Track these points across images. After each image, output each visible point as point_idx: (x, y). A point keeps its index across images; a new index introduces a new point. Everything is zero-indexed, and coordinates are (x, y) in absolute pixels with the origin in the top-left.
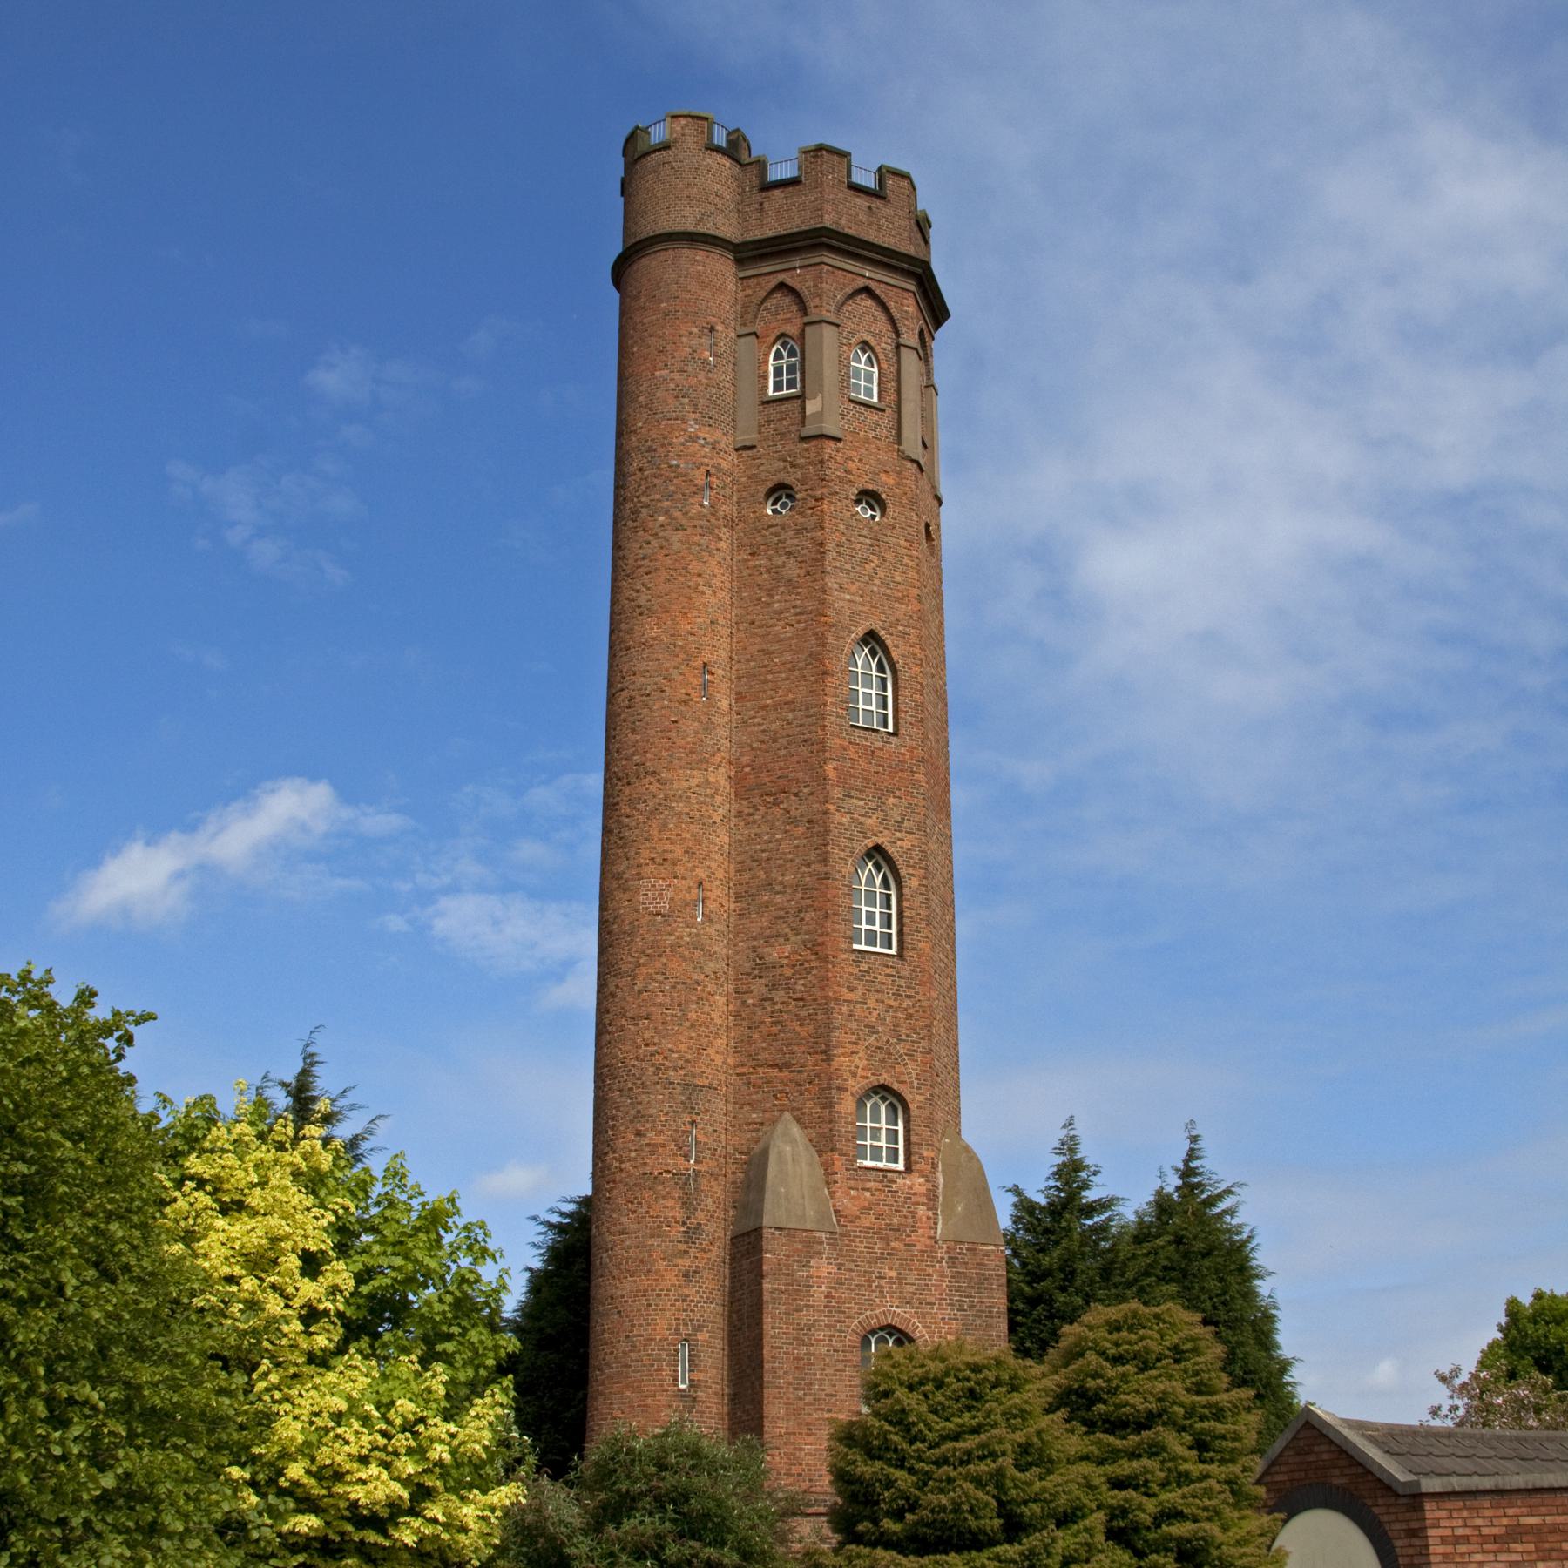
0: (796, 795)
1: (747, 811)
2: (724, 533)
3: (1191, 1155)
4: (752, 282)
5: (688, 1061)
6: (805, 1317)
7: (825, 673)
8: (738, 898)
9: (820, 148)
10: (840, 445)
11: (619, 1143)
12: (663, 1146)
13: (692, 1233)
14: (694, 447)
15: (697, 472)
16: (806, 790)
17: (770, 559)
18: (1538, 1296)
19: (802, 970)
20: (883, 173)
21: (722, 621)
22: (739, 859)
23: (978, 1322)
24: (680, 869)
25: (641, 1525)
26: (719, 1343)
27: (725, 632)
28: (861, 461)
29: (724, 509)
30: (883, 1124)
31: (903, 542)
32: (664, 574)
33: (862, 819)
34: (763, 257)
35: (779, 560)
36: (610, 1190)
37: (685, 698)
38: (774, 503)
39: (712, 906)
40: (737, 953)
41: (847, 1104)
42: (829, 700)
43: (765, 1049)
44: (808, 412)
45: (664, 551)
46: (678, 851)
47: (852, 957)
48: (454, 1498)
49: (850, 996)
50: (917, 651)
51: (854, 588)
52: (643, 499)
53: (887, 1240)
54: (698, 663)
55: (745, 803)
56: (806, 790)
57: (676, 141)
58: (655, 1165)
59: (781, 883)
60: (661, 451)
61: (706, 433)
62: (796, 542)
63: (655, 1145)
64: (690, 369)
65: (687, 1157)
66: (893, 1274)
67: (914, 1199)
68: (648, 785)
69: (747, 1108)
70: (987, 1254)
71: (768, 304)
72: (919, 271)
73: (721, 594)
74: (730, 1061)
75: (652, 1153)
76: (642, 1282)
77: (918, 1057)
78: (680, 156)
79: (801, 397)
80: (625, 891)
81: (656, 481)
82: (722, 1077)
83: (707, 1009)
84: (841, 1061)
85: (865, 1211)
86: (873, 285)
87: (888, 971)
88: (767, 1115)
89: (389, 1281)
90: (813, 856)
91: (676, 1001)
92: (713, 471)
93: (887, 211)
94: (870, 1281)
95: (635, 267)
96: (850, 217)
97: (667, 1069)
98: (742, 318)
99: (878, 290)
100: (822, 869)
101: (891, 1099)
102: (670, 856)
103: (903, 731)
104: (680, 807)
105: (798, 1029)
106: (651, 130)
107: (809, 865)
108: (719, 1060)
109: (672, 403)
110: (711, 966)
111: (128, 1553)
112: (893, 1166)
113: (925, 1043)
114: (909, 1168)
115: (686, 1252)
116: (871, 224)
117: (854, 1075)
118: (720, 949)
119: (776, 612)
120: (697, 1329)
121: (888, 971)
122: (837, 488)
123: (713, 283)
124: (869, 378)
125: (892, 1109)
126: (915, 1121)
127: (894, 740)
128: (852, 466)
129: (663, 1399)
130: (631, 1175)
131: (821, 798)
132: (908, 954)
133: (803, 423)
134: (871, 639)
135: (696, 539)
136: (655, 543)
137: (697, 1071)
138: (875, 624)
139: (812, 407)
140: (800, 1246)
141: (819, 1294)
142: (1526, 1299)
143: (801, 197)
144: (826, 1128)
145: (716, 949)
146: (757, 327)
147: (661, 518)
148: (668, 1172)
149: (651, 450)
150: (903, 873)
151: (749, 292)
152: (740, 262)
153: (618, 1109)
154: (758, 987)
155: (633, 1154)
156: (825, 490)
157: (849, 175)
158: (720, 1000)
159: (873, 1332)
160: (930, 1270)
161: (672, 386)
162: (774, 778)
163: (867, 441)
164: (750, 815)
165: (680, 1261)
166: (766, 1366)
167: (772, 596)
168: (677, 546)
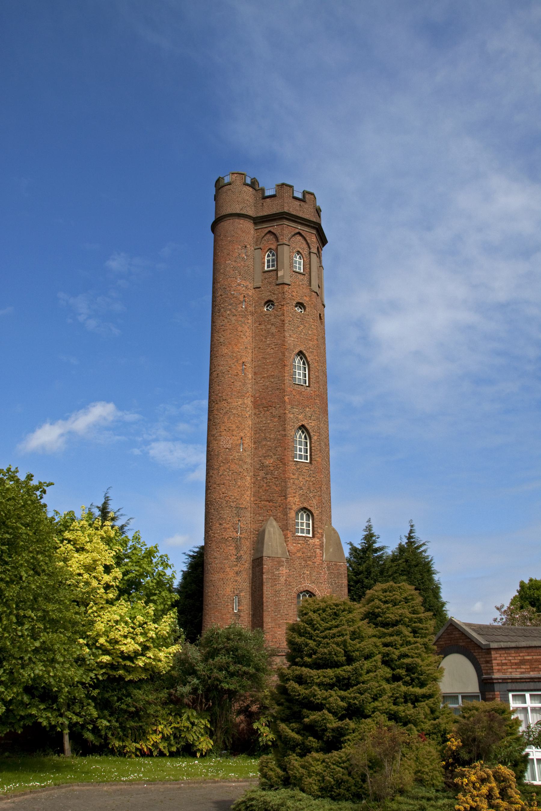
0: (275, 407)
1: (258, 413)
2: (250, 317)
3: (411, 532)
4: (260, 230)
5: (237, 499)
6: (278, 587)
7: (285, 365)
8: (255, 443)
9: (283, 184)
10: (290, 287)
11: (214, 528)
12: (229, 528)
13: (239, 558)
15: (240, 296)
17: (266, 326)
19: (277, 468)
20: (305, 193)
21: (249, 348)
22: (255, 429)
23: (338, 589)
24: (234, 433)
25: (221, 659)
27: (250, 351)
28: (297, 292)
29: (250, 309)
31: (311, 320)
32: (229, 331)
33: (297, 416)
35: (269, 327)
36: (211, 544)
37: (236, 374)
38: (267, 307)
39: (246, 446)
40: (254, 462)
41: (292, 514)
42: (286, 375)
43: (264, 495)
44: (279, 276)
45: (229, 323)
46: (234, 427)
47: (294, 463)
49: (293, 477)
51: (295, 336)
52: (222, 305)
53: (306, 561)
54: (241, 362)
55: (257, 410)
57: (233, 182)
58: (226, 535)
59: (269, 438)
60: (228, 289)
61: (243, 283)
62: (275, 320)
63: (226, 528)
65: (237, 532)
66: (308, 572)
67: (315, 547)
68: (224, 404)
69: (258, 515)
70: (341, 566)
71: (265, 238)
72: (317, 227)
73: (249, 338)
74: (252, 499)
75: (225, 531)
76: (221, 575)
77: (317, 498)
79: (276, 270)
80: (216, 441)
81: (226, 299)
82: (249, 505)
84: (290, 499)
85: (298, 551)
86: (301, 232)
87: (306, 468)
88: (265, 518)
89: (134, 575)
92: (246, 296)
93: (306, 206)
94: (300, 575)
96: (293, 208)
97: (230, 502)
98: (256, 243)
100: (283, 433)
101: (307, 512)
102: (231, 429)
103: (311, 385)
104: (234, 412)
105: (275, 488)
107: (279, 432)
108: (248, 499)
109: (232, 272)
110: (245, 466)
111: (44, 669)
112: (308, 535)
113: (319, 493)
114: (314, 536)
116: (300, 211)
117: (295, 504)
118: (249, 460)
120: (241, 592)
121: (306, 468)
122: (289, 302)
124: (300, 264)
125: (308, 516)
126: (316, 520)
127: (308, 388)
128: (294, 294)
129: (229, 616)
131: (283, 408)
132: (313, 462)
133: (277, 279)
134: (301, 354)
136: (226, 321)
137: (240, 502)
139: (280, 274)
140: (276, 563)
141: (283, 579)
143: (276, 201)
144: (285, 522)
146: (261, 246)
148: (230, 537)
149: (225, 288)
150: (312, 434)
151: (258, 234)
152: (255, 224)
153: (213, 516)
154: (262, 474)
155: (218, 531)
156: (285, 302)
157: (293, 194)
158: (248, 478)
159: (301, 593)
160: (321, 571)
164: (259, 414)
165: (235, 568)
166: (264, 604)
167: (266, 339)
168: (234, 321)
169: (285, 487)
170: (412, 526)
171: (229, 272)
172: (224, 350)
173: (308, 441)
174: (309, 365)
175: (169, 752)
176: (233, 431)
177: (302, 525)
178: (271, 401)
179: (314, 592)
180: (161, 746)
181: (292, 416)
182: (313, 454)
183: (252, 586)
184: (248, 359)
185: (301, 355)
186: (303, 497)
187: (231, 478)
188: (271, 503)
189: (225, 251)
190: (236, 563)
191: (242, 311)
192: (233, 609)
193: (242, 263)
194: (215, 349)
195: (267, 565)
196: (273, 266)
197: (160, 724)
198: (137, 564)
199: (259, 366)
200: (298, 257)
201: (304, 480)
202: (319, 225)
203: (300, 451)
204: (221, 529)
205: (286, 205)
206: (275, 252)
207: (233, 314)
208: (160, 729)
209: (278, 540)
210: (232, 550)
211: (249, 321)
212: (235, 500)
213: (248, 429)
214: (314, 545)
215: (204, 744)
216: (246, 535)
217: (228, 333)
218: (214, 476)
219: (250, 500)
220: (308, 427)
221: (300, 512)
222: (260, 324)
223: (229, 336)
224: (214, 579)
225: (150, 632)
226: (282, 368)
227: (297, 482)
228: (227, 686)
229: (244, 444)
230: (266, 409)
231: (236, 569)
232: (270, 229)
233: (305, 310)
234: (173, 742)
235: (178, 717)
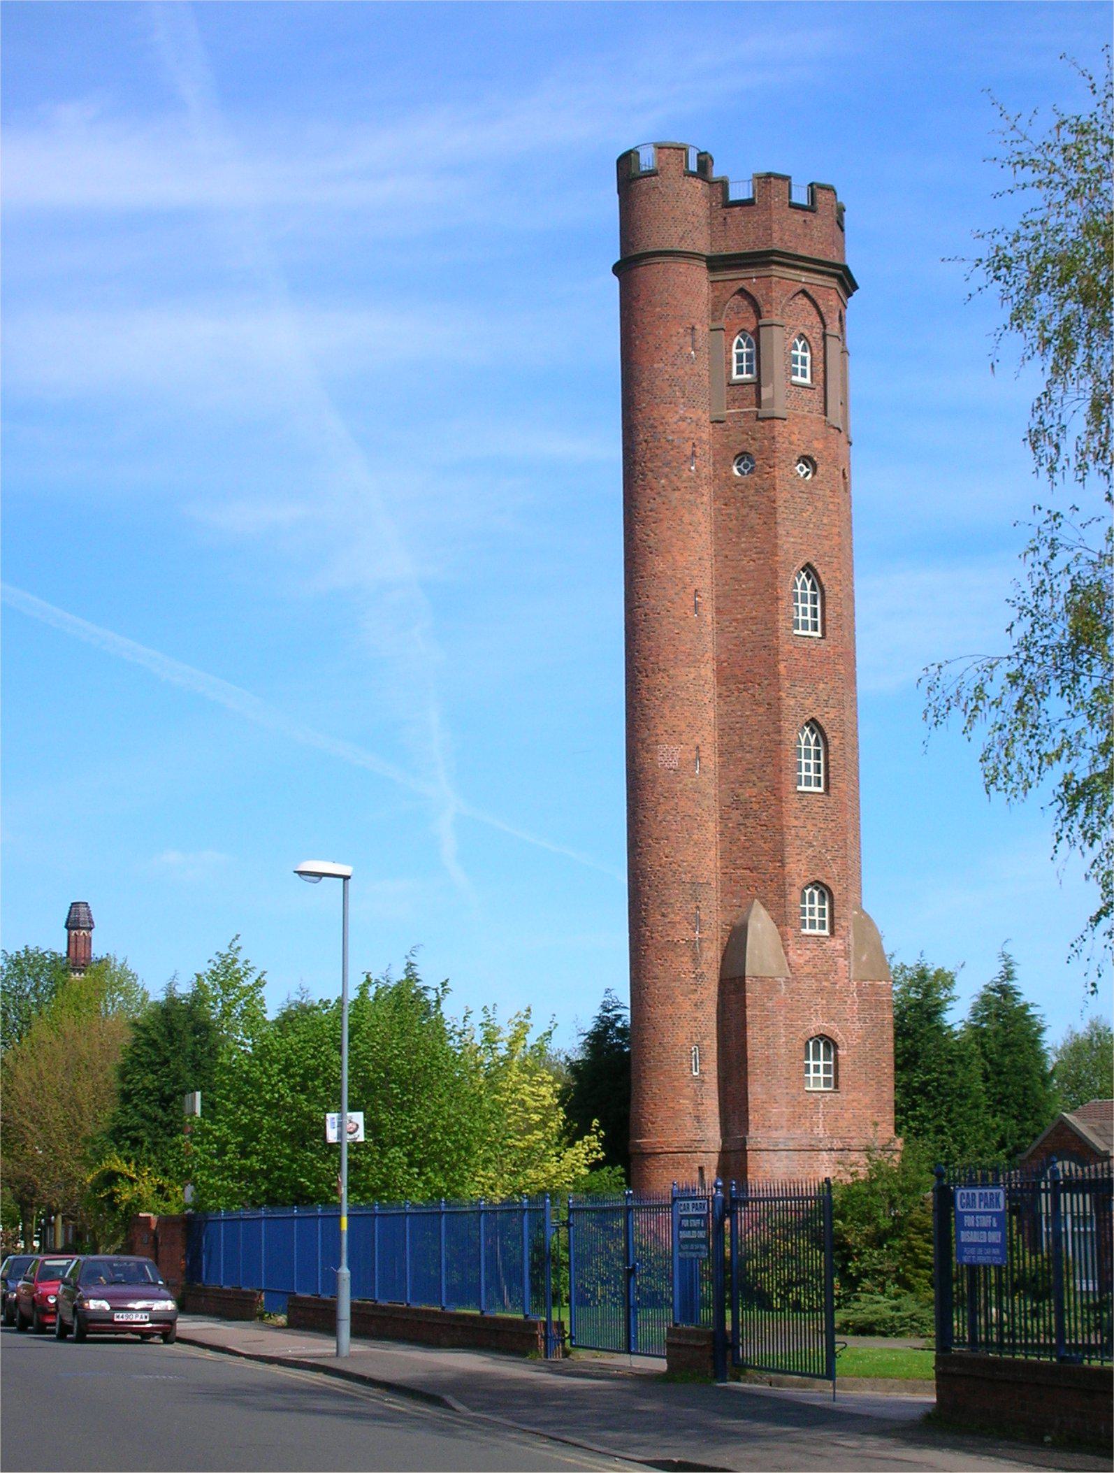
9: (769, 175)
20: (813, 188)
21: (706, 557)
35: (745, 511)
38: (739, 464)
41: (794, 895)
46: (683, 726)
49: (796, 823)
51: (796, 532)
52: (649, 465)
60: (660, 429)
68: (660, 679)
73: (704, 537)
79: (758, 385)
86: (807, 287)
100: (777, 738)
101: (821, 888)
103: (828, 635)
107: (768, 735)
108: (712, 866)
113: (842, 851)
118: (712, 791)
120: (703, 1038)
123: (690, 291)
126: (836, 903)
132: (832, 791)
133: (759, 405)
139: (766, 393)
150: (829, 736)
154: (736, 815)
157: (790, 197)
166: (749, 1062)
172: (659, 565)
174: (823, 592)
177: (812, 913)
178: (752, 669)
181: (792, 703)
182: (831, 775)
189: (650, 338)
190: (694, 987)
191: (690, 479)
195: (753, 992)
196: (749, 371)
199: (726, 597)
201: (815, 829)
202: (846, 269)
203: (808, 769)
205: (775, 227)
206: (755, 337)
211: (705, 499)
220: (822, 722)
221: (807, 888)
227: (802, 832)
230: (741, 686)
232: (742, 284)
233: (814, 473)
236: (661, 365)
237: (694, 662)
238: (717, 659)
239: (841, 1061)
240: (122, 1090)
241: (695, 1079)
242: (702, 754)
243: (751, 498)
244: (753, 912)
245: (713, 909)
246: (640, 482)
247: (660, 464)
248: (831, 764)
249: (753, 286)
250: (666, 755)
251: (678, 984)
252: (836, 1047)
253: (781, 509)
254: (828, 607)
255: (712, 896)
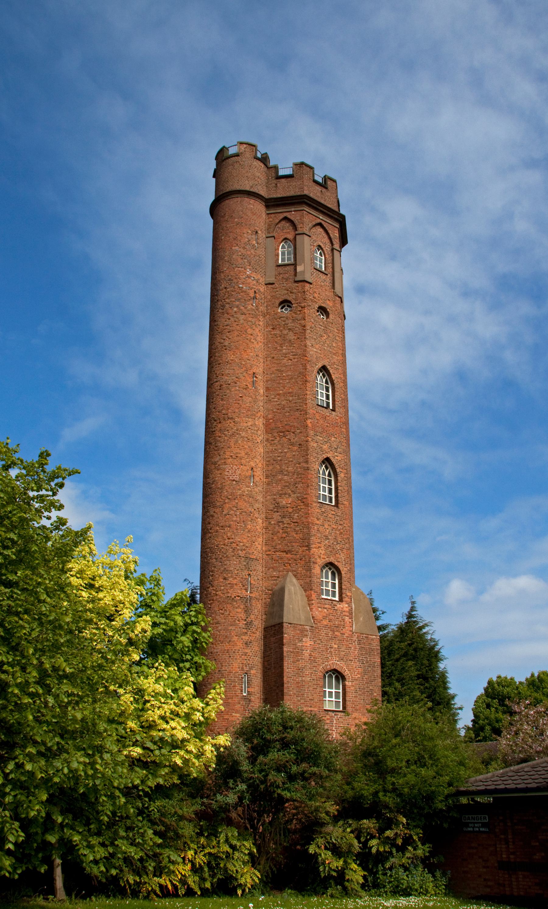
0: (293, 433)
1: (271, 439)
2: (261, 318)
3: (413, 609)
4: (272, 216)
5: (247, 547)
6: (301, 664)
7: (306, 381)
8: (267, 477)
9: (302, 164)
10: (311, 286)
11: (215, 583)
12: (236, 584)
13: (249, 625)
14: (249, 281)
15: (250, 291)
16: (298, 431)
17: (281, 331)
18: (499, 677)
19: (297, 509)
20: (326, 178)
21: (260, 356)
22: (267, 459)
23: (370, 669)
24: (243, 461)
25: (275, 755)
26: (260, 675)
27: (262, 360)
28: (319, 293)
29: (262, 308)
30: (330, 580)
31: (336, 330)
32: (236, 333)
33: (321, 445)
34: (278, 206)
35: (285, 332)
36: (211, 604)
37: (245, 387)
38: (282, 308)
39: (257, 479)
40: (267, 501)
41: (317, 570)
42: (308, 393)
43: (279, 544)
44: (298, 271)
45: (236, 323)
46: (243, 454)
47: (318, 505)
48: (197, 740)
49: (318, 522)
50: (342, 376)
51: (317, 347)
52: (227, 300)
53: (333, 631)
54: (251, 372)
55: (270, 435)
56: (298, 431)
57: (242, 153)
58: (232, 593)
59: (287, 471)
60: (235, 281)
61: (254, 275)
62: (293, 324)
63: (233, 584)
64: (247, 247)
65: (246, 590)
66: (336, 646)
67: (344, 613)
68: (229, 424)
69: (271, 570)
70: (372, 640)
71: (279, 225)
72: (341, 220)
73: (260, 344)
74: (264, 548)
75: (231, 587)
76: (226, 646)
77: (345, 551)
78: (244, 159)
79: (295, 265)
80: (218, 470)
81: (233, 293)
82: (261, 555)
83: (255, 524)
84: (314, 550)
85: (325, 618)
86: (323, 223)
87: (333, 512)
88: (281, 573)
89: (161, 631)
90: (302, 460)
91: (242, 520)
92: (257, 292)
93: (328, 194)
94: (327, 649)
95: (223, 204)
96: (315, 192)
97: (238, 550)
98: (268, 230)
99: (325, 225)
100: (305, 465)
101: (333, 569)
102: (239, 455)
103: (337, 410)
104: (243, 434)
105: (295, 535)
106: (230, 149)
107: (299, 464)
108: (260, 547)
109: (240, 261)
110: (257, 505)
111: (87, 761)
112: (334, 599)
113: (347, 545)
114: (341, 600)
115: (246, 633)
117: (320, 557)
118: (260, 498)
119: (284, 354)
120: (251, 668)
121: (333, 512)
122: (310, 304)
123: (253, 215)
124: (321, 262)
125: (333, 574)
126: (344, 579)
127: (333, 413)
128: (316, 295)
129: (236, 700)
130: (221, 597)
131: (305, 435)
132: (340, 506)
133: (295, 275)
134: (324, 369)
135: (250, 319)
136: (232, 319)
137: (251, 552)
138: (326, 363)
139: (299, 269)
140: (299, 632)
141: (306, 653)
142: (495, 679)
143: (293, 183)
144: (308, 580)
145: (258, 498)
146: (274, 234)
147: (235, 309)
148: (238, 596)
149: (230, 280)
150: (338, 470)
151: (270, 220)
152: (267, 207)
153: (215, 567)
154: (276, 516)
155: (222, 588)
156: (306, 304)
157: (313, 176)
158: (260, 521)
159: (327, 672)
160: (350, 645)
161: (240, 254)
162: (283, 425)
163: (321, 286)
164: (272, 440)
165: (244, 637)
166: (285, 685)
167: (282, 347)
168: (242, 322)
169: (308, 534)
170: (413, 603)
171: (237, 260)
172: (230, 356)
173: (333, 479)
175: (201, 889)
176: (241, 459)
178: (288, 425)
179: (342, 672)
180: (190, 881)
181: (315, 445)
183: (264, 661)
184: (259, 370)
185: (324, 372)
186: (330, 549)
187: (238, 519)
188: (289, 555)
189: (231, 235)
190: (245, 631)
192: (242, 691)
193: (252, 251)
194: (217, 354)
195: (288, 634)
197: (189, 849)
198: (163, 615)
200: (318, 253)
204: (226, 585)
207: (241, 311)
208: (190, 857)
209: (300, 602)
210: (241, 613)
212: (244, 547)
213: (259, 457)
214: (342, 612)
215: (248, 876)
216: (257, 594)
217: (235, 335)
218: (216, 516)
219: (262, 549)
220: (333, 460)
222: (273, 329)
223: (236, 339)
224: (215, 651)
225: (196, 712)
226: (303, 384)
227: (322, 528)
228: (288, 794)
229: (255, 477)
231: (246, 638)
234: (206, 875)
235: (213, 838)
236: (237, 248)
237: (252, 415)
238: (265, 417)
239: (348, 690)
240: (236, 763)
241: (244, 698)
242: (255, 473)
243: (290, 325)
244: (288, 579)
245: (260, 578)
246: (220, 311)
247: (233, 300)
248: (340, 488)
249: (292, 216)
250: (231, 471)
251: (233, 628)
252: (344, 678)
253: (308, 331)
254: (337, 394)
255: (259, 569)
